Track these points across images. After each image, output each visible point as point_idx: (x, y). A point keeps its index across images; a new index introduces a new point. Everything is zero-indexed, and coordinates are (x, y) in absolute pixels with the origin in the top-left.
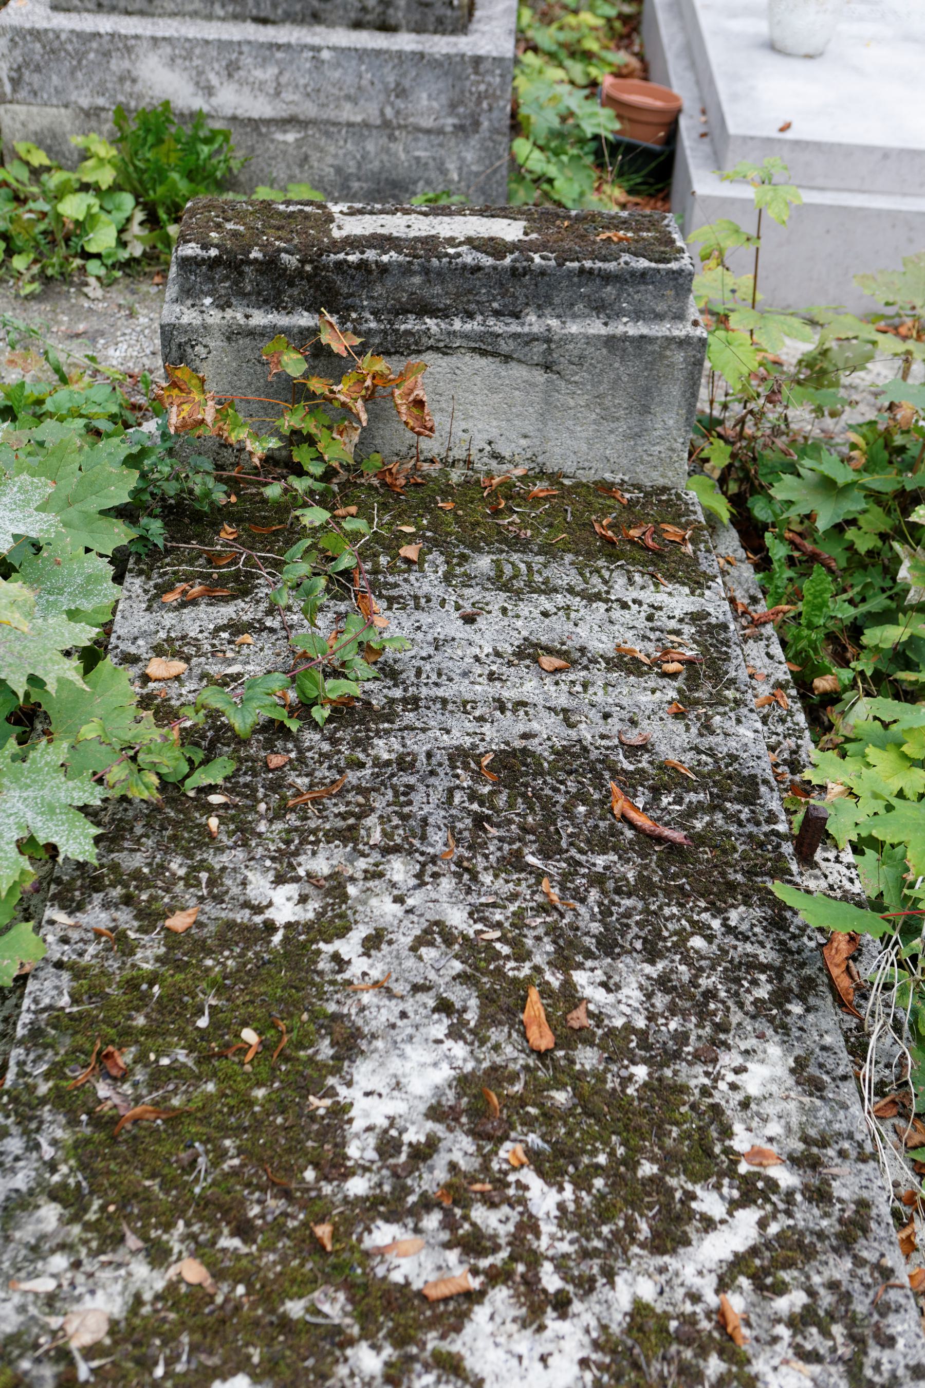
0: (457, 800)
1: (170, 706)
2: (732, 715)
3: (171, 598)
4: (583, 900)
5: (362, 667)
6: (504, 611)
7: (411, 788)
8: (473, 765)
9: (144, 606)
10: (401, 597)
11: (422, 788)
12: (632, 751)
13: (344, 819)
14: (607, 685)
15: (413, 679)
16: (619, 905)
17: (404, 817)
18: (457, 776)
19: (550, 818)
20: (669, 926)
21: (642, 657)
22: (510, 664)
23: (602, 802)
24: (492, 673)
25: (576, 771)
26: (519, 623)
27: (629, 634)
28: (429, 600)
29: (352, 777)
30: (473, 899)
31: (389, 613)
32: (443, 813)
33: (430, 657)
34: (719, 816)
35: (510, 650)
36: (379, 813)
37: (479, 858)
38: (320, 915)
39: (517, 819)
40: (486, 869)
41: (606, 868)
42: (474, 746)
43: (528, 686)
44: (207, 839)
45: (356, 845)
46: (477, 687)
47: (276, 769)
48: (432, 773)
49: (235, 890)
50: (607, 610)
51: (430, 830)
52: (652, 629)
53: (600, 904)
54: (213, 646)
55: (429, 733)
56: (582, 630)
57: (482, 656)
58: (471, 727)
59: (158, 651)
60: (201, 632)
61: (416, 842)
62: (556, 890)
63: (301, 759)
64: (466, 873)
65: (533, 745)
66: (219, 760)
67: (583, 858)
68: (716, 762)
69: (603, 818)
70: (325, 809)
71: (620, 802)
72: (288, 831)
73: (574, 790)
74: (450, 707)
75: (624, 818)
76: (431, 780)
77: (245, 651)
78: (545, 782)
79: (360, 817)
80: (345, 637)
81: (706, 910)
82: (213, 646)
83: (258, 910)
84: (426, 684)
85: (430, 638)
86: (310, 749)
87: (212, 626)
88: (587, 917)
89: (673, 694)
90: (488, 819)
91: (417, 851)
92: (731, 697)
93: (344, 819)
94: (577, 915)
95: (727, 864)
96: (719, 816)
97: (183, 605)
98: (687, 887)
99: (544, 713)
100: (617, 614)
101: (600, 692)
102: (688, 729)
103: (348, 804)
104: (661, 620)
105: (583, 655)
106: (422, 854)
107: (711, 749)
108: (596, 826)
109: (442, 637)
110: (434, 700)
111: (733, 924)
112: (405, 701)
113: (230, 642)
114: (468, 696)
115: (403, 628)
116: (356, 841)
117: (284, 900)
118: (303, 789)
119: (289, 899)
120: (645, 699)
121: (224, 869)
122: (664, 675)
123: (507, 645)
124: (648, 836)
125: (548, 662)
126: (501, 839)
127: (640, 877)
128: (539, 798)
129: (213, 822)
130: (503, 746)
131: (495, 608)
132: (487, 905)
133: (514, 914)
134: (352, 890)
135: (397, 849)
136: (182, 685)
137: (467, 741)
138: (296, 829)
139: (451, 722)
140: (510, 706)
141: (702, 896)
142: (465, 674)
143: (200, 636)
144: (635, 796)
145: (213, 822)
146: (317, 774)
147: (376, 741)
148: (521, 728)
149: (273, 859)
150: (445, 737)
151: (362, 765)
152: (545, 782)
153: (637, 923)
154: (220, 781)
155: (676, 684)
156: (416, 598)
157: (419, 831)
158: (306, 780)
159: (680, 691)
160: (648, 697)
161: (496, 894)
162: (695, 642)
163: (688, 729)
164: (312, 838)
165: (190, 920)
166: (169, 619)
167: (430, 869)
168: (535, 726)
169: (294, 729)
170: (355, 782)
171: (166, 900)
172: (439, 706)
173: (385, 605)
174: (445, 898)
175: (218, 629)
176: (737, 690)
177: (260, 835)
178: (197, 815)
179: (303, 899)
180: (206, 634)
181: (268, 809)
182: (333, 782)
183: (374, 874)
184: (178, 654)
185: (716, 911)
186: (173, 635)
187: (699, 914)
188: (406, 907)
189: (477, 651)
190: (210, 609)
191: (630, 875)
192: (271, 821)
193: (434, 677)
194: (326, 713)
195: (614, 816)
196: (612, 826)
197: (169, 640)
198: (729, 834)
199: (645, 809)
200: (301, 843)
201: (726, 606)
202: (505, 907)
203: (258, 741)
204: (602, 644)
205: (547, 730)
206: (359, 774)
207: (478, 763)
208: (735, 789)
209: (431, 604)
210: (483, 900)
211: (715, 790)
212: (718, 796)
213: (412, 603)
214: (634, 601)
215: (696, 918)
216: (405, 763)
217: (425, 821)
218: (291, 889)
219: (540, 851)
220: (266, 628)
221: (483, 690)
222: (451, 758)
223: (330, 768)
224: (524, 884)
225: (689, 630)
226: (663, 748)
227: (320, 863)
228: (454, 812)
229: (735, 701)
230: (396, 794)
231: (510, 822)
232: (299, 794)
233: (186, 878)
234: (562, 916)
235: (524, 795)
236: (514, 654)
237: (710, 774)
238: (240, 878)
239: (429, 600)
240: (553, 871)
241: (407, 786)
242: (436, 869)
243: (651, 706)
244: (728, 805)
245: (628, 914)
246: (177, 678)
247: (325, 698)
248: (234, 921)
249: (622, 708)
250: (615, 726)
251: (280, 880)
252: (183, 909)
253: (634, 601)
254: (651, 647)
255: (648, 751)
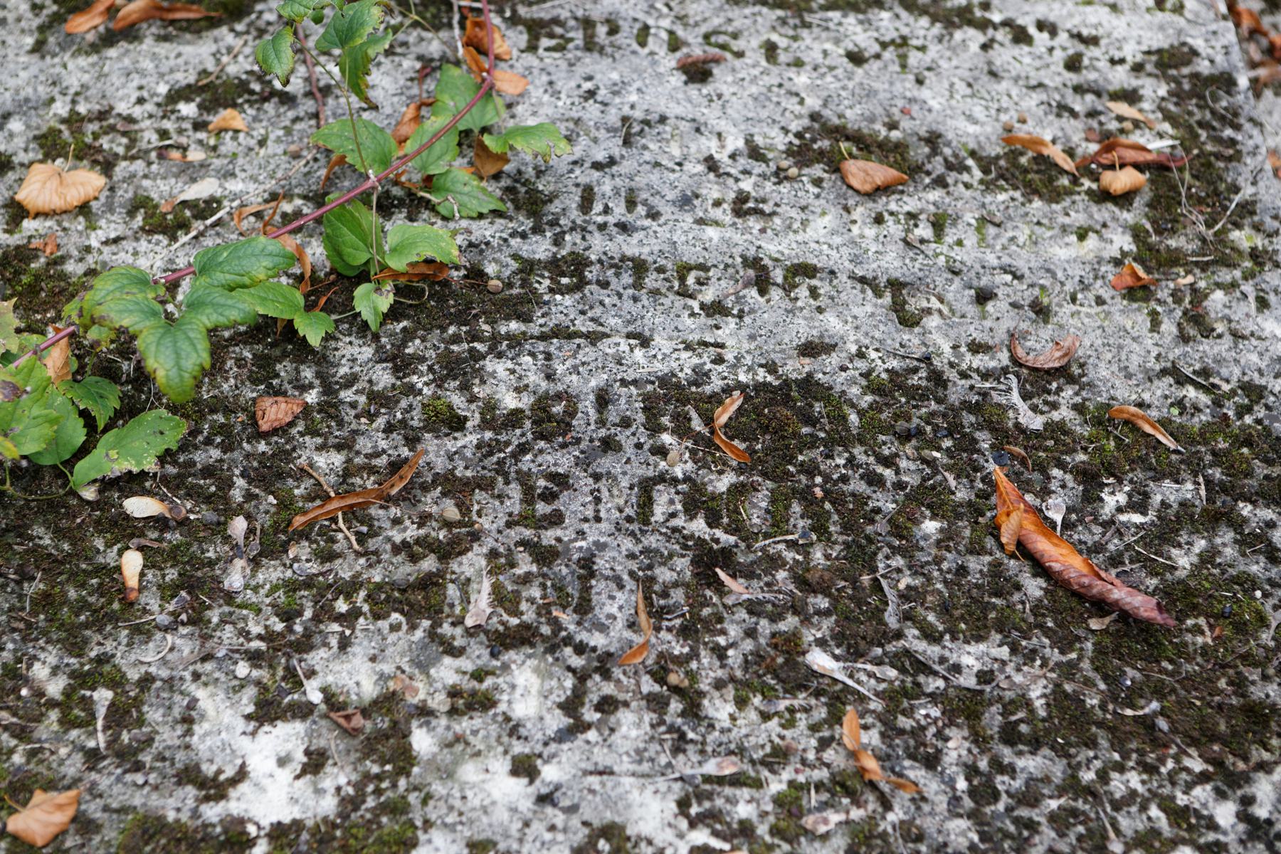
0: (659, 512)
1: (63, 276)
2: (1248, 288)
3: (86, 24)
4: (932, 762)
5: (467, 188)
6: (771, 50)
7: (561, 481)
8: (697, 424)
9: (29, 41)
10: (556, 21)
11: (584, 482)
12: (1039, 382)
13: (414, 559)
14: (983, 221)
15: (575, 214)
16: (1011, 770)
17: (544, 556)
18: (662, 451)
19: (860, 555)
20: (1124, 822)
21: (1056, 153)
22: (780, 176)
23: (975, 510)
24: (742, 198)
25: (920, 432)
26: (802, 80)
27: (1031, 102)
28: (613, 30)
29: (435, 452)
30: (687, 765)
31: (530, 59)
32: (628, 544)
33: (612, 162)
34: (1226, 536)
35: (781, 141)
36: (489, 543)
37: (706, 658)
38: (350, 803)
39: (789, 556)
40: (719, 685)
41: (985, 677)
42: (701, 376)
43: (817, 227)
44: (115, 606)
45: (437, 624)
46: (711, 233)
47: (275, 431)
48: (609, 445)
49: (168, 736)
50: (985, 47)
51: (598, 585)
52: (1079, 89)
53: (971, 771)
54: (164, 134)
55: (606, 346)
56: (932, 95)
57: (722, 157)
58: (693, 327)
59: (50, 146)
60: (141, 101)
61: (567, 619)
62: (872, 738)
63: (330, 408)
64: (677, 700)
65: (826, 369)
66: (149, 416)
67: (931, 651)
68: (1217, 403)
69: (976, 549)
70: (373, 533)
71: (1015, 517)
72: (291, 587)
73: (912, 480)
74: (651, 280)
75: (1023, 550)
76: (606, 463)
77: (228, 145)
78: (851, 462)
79: (448, 552)
80: (435, 123)
81: (1203, 778)
82: (164, 134)
83: (215, 789)
84: (602, 227)
85: (613, 117)
86: (351, 381)
87: (163, 89)
88: (942, 803)
89: (1122, 242)
90: (725, 557)
91: (568, 641)
92: (1245, 245)
93: (414, 559)
94: (920, 799)
95: (1247, 658)
96: (1226, 536)
97: (109, 39)
98: (1163, 724)
99: (851, 293)
100: (1006, 54)
101: (971, 240)
102: (1155, 325)
103: (424, 519)
104: (1099, 70)
105: (935, 151)
106: (580, 649)
107: (1205, 372)
108: (962, 571)
109: (638, 114)
110: (619, 264)
111: (1262, 812)
112: (555, 266)
113: (199, 126)
114: (691, 255)
115: (556, 94)
116: (435, 612)
117: (272, 763)
118: (329, 482)
119: (282, 762)
120: (1065, 252)
121: (147, 680)
122: (1103, 196)
123: (775, 132)
124: (1075, 594)
125: (865, 172)
126: (753, 608)
127: (1057, 698)
128: (838, 500)
129: (132, 563)
130: (762, 375)
131: (751, 45)
132: (720, 780)
133: (778, 800)
134: (422, 741)
135: (521, 638)
136: (92, 227)
137: (686, 363)
138: (309, 583)
139: (652, 319)
140: (778, 275)
141: (1194, 742)
142: (686, 201)
143: (137, 112)
144: (1045, 493)
145: (132, 563)
146: (364, 445)
147: (490, 364)
148: (802, 329)
149: (254, 658)
150: (639, 354)
151: (457, 424)
152: (851, 462)
153: (1052, 818)
154: (150, 465)
155: (1128, 217)
156: (587, 24)
157: (573, 590)
158: (337, 459)
159: (1137, 233)
160: (1074, 247)
161: (740, 751)
162: (1168, 117)
163: (1155, 325)
164: (342, 606)
165: (61, 818)
166: (76, 71)
167: (599, 688)
168: (832, 323)
169: (314, 340)
170: (441, 465)
171: (18, 759)
172: (627, 279)
173: (523, 39)
174: (625, 765)
175: (176, 95)
176: (1257, 228)
177: (229, 597)
178: (99, 543)
179: (315, 763)
180: (149, 107)
181: (251, 531)
182: (396, 466)
183: (468, 700)
184: (89, 155)
185: (1229, 781)
186: (82, 109)
187: (1188, 789)
188: (540, 787)
189: (709, 145)
190: (163, 49)
191: (1036, 693)
192: (255, 563)
193: (619, 210)
194: (385, 302)
195: (1002, 546)
196: (996, 567)
197: (74, 120)
198: (1248, 583)
199: (1067, 525)
200: (317, 619)
201: (1229, 34)
202: (758, 784)
203: (240, 362)
204: (972, 125)
205: (856, 332)
206: (451, 445)
207: (709, 420)
208: (1261, 470)
209: (620, 39)
210: (711, 767)
211: (1217, 473)
212: (1224, 489)
213: (578, 36)
214: (1041, 26)
215: (1182, 799)
216: (550, 420)
217: (587, 564)
218: (288, 736)
219: (839, 638)
220: (274, 93)
221: (723, 238)
222: (651, 408)
223: (389, 429)
224: (802, 721)
225: (1154, 90)
226: (1104, 372)
227: (352, 671)
228: (652, 541)
229: (1255, 254)
230: (529, 496)
231: (775, 562)
232: (317, 494)
233: (64, 704)
234: (887, 806)
235: (805, 496)
236: (789, 152)
237: (1205, 434)
238: (180, 702)
239: (613, 30)
240: (867, 687)
241: (553, 477)
242: (608, 689)
243: (1077, 272)
244: (1245, 509)
245: (1029, 797)
246: (84, 209)
247: (384, 267)
248: (161, 819)
249: (1017, 277)
250: (1001, 319)
251: (267, 711)
252: (51, 785)
253: (1041, 26)
254: (1075, 131)
255: (1072, 380)
